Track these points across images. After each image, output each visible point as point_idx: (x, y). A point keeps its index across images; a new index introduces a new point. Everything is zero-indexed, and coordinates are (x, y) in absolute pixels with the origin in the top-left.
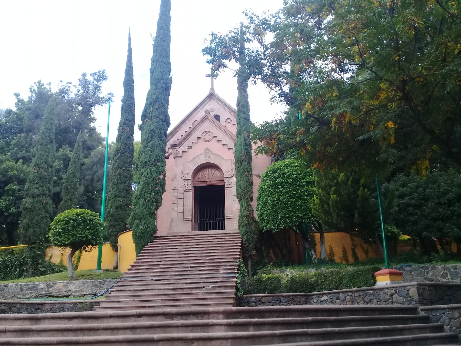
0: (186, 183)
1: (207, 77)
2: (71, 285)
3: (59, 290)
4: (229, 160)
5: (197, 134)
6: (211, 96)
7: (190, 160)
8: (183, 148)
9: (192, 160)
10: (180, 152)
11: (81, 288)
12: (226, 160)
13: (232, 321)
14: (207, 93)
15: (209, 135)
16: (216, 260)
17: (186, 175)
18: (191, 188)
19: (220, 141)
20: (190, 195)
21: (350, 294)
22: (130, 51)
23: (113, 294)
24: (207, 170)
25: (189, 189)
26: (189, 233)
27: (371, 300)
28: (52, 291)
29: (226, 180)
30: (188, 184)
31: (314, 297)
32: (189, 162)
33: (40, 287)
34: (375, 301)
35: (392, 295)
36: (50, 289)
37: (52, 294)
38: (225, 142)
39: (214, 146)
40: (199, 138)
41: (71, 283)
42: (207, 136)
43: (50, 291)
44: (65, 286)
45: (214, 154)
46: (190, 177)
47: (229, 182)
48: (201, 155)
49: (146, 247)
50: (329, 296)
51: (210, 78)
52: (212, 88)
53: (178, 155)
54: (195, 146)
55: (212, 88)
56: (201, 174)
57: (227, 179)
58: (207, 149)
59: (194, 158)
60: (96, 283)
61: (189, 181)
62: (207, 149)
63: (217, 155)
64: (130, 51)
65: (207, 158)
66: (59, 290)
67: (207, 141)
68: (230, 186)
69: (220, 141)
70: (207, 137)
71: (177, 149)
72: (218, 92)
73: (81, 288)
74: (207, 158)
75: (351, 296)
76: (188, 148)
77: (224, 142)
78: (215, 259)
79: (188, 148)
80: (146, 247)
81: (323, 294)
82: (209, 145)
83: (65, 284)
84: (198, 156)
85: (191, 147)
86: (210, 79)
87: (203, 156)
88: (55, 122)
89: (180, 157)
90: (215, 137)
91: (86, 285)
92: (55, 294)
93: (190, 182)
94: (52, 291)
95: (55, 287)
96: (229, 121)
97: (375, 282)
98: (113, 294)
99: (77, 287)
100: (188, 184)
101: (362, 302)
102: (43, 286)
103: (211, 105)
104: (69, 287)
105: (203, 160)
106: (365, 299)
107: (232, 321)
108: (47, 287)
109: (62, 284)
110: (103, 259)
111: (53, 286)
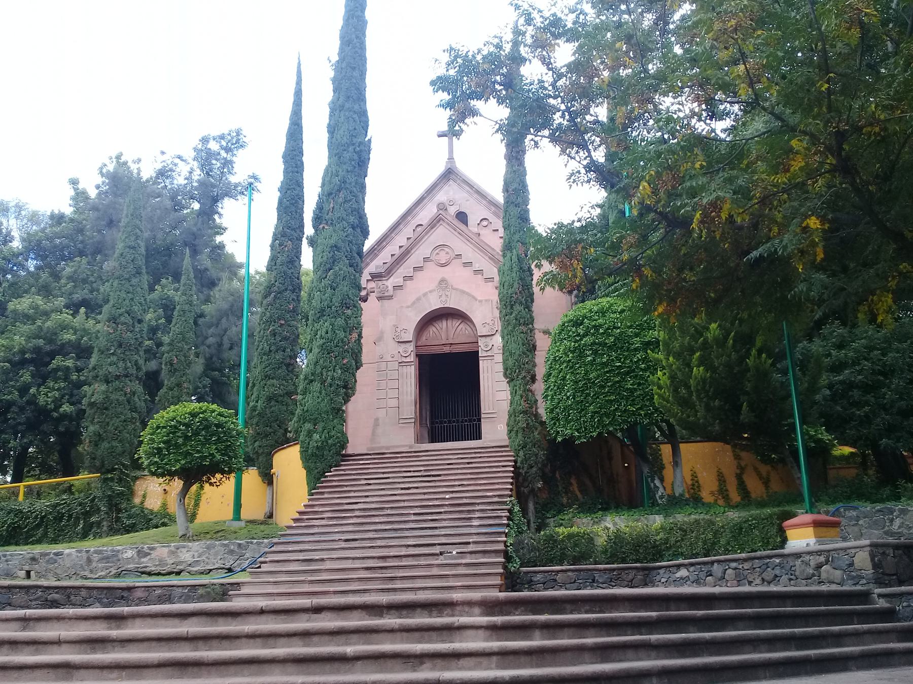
0: (401, 348)
1: (439, 136)
2: (184, 550)
4: (486, 300)
6: (450, 174)
7: (409, 304)
9: (414, 303)
10: (390, 288)
12: (480, 301)
13: (498, 619)
14: (441, 169)
16: (465, 501)
18: (412, 358)
19: (468, 264)
20: (411, 372)
21: (734, 565)
22: (298, 94)
23: (265, 568)
24: (444, 323)
25: (408, 360)
26: (411, 447)
27: (776, 576)
29: (481, 342)
31: (662, 571)
32: (408, 307)
33: (125, 556)
34: (785, 578)
35: (819, 567)
36: (143, 560)
37: (148, 570)
38: (477, 265)
40: (426, 260)
42: (442, 254)
43: (143, 563)
44: (173, 553)
46: (410, 336)
47: (487, 346)
48: (431, 292)
49: (327, 476)
50: (692, 569)
51: (446, 139)
52: (451, 158)
53: (386, 294)
54: (419, 274)
55: (451, 158)
56: (432, 330)
59: (418, 299)
60: (232, 547)
61: (408, 344)
62: (443, 281)
63: (463, 292)
65: (443, 298)
66: (160, 561)
67: (443, 265)
68: (489, 353)
69: (468, 264)
70: (443, 257)
72: (463, 166)
75: (735, 569)
76: (408, 278)
77: (477, 266)
79: (408, 278)
80: (327, 476)
83: (172, 549)
84: (425, 295)
85: (411, 278)
87: (435, 293)
88: (145, 235)
89: (390, 298)
91: (213, 551)
92: (153, 569)
93: (411, 347)
94: (148, 563)
95: (154, 554)
96: (485, 223)
97: (784, 540)
98: (265, 568)
101: (758, 581)
102: (129, 554)
103: (450, 193)
104: (180, 555)
105: (434, 304)
106: (764, 575)
107: (498, 619)
109: (166, 550)
111: (149, 554)
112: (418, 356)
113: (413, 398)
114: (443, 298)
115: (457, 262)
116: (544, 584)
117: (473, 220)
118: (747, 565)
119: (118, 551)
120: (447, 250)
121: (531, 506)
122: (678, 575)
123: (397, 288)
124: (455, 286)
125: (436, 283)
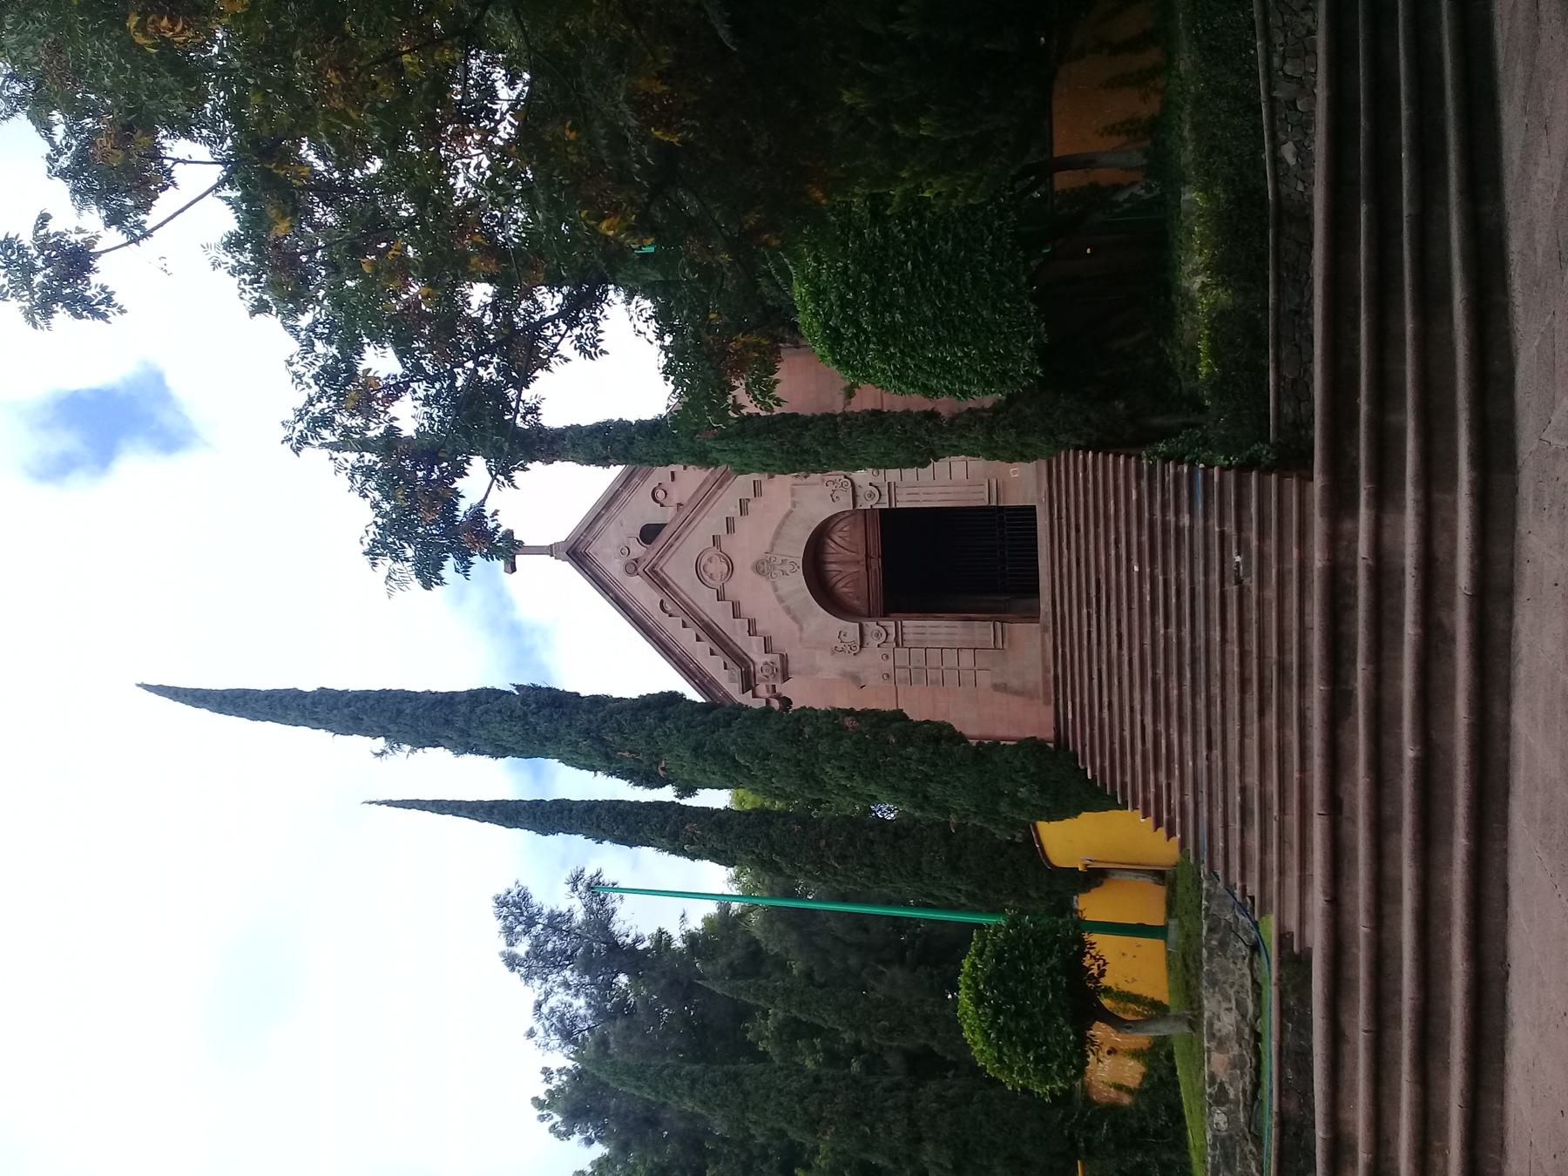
0: (872, 642)
1: (514, 569)
2: (1217, 1025)
3: (1234, 1067)
4: (793, 495)
5: (705, 601)
7: (795, 626)
8: (754, 650)
9: (794, 618)
10: (768, 658)
11: (1231, 992)
12: (794, 504)
14: (566, 569)
17: (846, 639)
19: (730, 525)
21: (1276, 61)
22: (390, 803)
23: (1253, 888)
25: (892, 631)
26: (1045, 630)
28: (1236, 1090)
30: (878, 635)
31: (1284, 190)
32: (801, 629)
33: (1223, 1126)
36: (1232, 1096)
37: (1249, 1088)
38: (732, 509)
39: (749, 543)
40: (721, 597)
41: (1211, 1025)
42: (711, 568)
43: (1236, 1096)
44: (1221, 1044)
45: (773, 545)
46: (852, 628)
47: (871, 495)
48: (776, 590)
50: (1282, 137)
52: (551, 550)
53: (778, 666)
54: (746, 609)
55: (551, 550)
58: (758, 568)
59: (788, 610)
60: (1214, 942)
61: (868, 631)
62: (758, 568)
63: (777, 534)
64: (390, 803)
65: (788, 568)
66: (1234, 1067)
67: (731, 568)
68: (885, 491)
69: (730, 525)
71: (758, 668)
72: (561, 530)
74: (788, 568)
75: (1284, 59)
76: (752, 630)
77: (734, 511)
79: (752, 630)
81: (1277, 160)
82: (743, 563)
84: (781, 600)
86: (520, 560)
89: (784, 659)
91: (1220, 977)
92: (1247, 1079)
93: (871, 626)
95: (1222, 1076)
96: (660, 494)
99: (1225, 1005)
101: (1308, 18)
103: (609, 553)
104: (1225, 1031)
105: (795, 584)
109: (1215, 1056)
110: (1131, 919)
111: (1222, 1084)
112: (886, 614)
113: (958, 623)
115: (726, 543)
116: (1300, 401)
120: (704, 560)
124: (768, 548)
125: (762, 580)
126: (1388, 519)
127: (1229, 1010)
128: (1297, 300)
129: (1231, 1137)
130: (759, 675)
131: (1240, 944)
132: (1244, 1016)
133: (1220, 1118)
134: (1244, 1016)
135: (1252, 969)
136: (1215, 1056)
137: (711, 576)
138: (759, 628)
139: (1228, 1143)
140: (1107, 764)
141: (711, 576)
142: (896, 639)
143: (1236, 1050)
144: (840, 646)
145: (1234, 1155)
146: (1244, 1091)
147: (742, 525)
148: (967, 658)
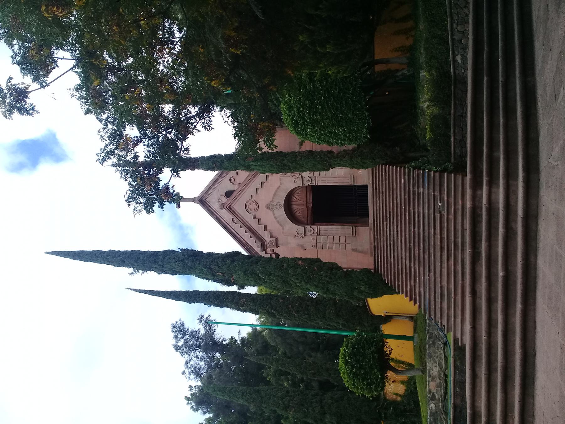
0: (309, 234)
1: (179, 207)
2: (432, 372)
3: (438, 387)
4: (280, 180)
7: (281, 228)
9: (281, 225)
10: (271, 239)
11: (437, 360)
12: (281, 184)
13: (421, 186)
14: (198, 207)
15: (250, 204)
16: (407, 197)
19: (258, 191)
20: (323, 228)
21: (455, 26)
22: (135, 290)
23: (445, 323)
25: (316, 230)
26: (371, 229)
28: (439, 395)
29: (306, 184)
30: (311, 231)
31: (457, 72)
32: (283, 229)
33: (434, 408)
37: (443, 395)
38: (258, 185)
40: (254, 217)
41: (429, 372)
42: (251, 207)
44: (433, 379)
45: (273, 199)
46: (301, 228)
47: (308, 180)
48: (274, 215)
50: (456, 53)
52: (193, 200)
54: (263, 222)
55: (193, 200)
57: (305, 182)
58: (268, 207)
59: (278, 222)
61: (307, 230)
62: (268, 207)
63: (275, 195)
64: (135, 290)
65: (278, 207)
66: (438, 387)
67: (258, 207)
68: (313, 179)
69: (258, 191)
70: (253, 206)
71: (267, 243)
72: (196, 193)
73: (437, 360)
75: (457, 25)
76: (265, 229)
77: (259, 186)
78: (405, 199)
79: (265, 229)
81: (455, 61)
82: (262, 205)
83: (430, 379)
84: (276, 218)
87: (276, 212)
89: (277, 240)
90: (252, 197)
92: (443, 391)
93: (308, 228)
95: (434, 390)
96: (232, 180)
99: (434, 365)
100: (311, 231)
101: (466, 10)
104: (434, 374)
105: (281, 212)
108: (434, 400)
109: (431, 383)
111: (433, 393)
112: (313, 224)
113: (340, 227)
114: (278, 207)
116: (462, 148)
117: (230, 187)
118: (456, 17)
119: (431, 412)
121: (412, 155)
122: (460, 61)
123: (271, 235)
124: (271, 200)
126: (494, 190)
127: (436, 366)
128: (462, 111)
129: (436, 412)
130: (268, 245)
131: (440, 343)
132: (441, 369)
133: (433, 406)
134: (441, 369)
135: (444, 352)
136: (431, 383)
137: (251, 210)
138: (268, 228)
139: (435, 415)
140: (393, 278)
141: (251, 210)
142: (317, 233)
143: (438, 381)
144: (297, 235)
145: (437, 419)
146: (441, 396)
147: (262, 191)
148: (343, 239)
